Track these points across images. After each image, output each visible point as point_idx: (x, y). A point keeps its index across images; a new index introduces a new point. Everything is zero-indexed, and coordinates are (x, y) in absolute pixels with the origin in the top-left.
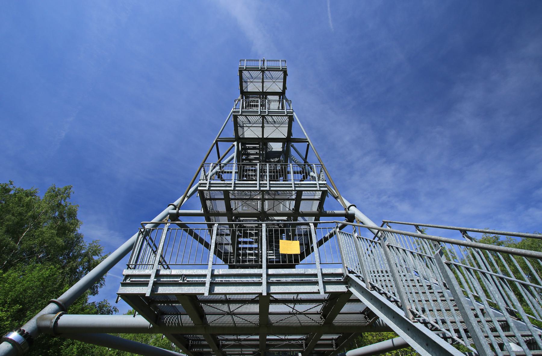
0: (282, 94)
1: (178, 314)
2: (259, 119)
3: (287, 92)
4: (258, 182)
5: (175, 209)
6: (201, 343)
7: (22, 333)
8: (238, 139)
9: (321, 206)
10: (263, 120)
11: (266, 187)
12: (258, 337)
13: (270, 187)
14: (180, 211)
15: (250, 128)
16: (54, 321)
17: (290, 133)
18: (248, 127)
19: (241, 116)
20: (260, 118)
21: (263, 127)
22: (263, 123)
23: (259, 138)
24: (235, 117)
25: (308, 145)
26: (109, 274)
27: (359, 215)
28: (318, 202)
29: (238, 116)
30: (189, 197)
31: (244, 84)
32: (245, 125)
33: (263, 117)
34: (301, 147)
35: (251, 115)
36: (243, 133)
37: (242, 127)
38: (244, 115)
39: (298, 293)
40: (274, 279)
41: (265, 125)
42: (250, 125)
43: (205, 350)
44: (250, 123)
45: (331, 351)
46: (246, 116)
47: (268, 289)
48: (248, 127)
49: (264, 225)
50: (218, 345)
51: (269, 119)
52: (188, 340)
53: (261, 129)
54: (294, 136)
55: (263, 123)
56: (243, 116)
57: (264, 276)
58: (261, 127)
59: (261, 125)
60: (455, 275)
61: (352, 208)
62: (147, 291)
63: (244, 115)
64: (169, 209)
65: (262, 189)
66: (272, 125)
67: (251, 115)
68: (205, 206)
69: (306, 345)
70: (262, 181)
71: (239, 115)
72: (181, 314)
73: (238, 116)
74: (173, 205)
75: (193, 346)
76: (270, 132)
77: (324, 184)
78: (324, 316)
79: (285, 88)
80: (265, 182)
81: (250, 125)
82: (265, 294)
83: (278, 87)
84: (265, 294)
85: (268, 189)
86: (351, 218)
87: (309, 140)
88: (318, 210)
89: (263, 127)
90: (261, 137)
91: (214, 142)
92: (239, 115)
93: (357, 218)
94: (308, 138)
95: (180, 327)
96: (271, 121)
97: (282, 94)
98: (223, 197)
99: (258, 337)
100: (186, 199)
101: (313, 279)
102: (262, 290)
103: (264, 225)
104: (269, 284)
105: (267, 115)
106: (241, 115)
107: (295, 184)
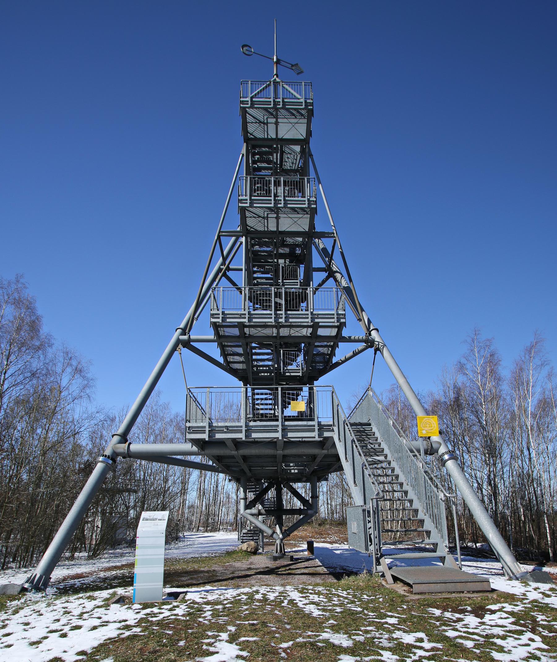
0: (304, 143)
3: (312, 140)
6: (278, 333)
7: (278, 333)
8: (247, 231)
12: (287, 107)
17: (312, 225)
26: (134, 429)
39: (302, 438)
49: (280, 389)
54: (318, 229)
57: (280, 427)
58: (276, 218)
60: (443, 435)
79: (309, 133)
97: (304, 143)
98: (212, 337)
99: (287, 107)
101: (271, 316)
103: (280, 389)
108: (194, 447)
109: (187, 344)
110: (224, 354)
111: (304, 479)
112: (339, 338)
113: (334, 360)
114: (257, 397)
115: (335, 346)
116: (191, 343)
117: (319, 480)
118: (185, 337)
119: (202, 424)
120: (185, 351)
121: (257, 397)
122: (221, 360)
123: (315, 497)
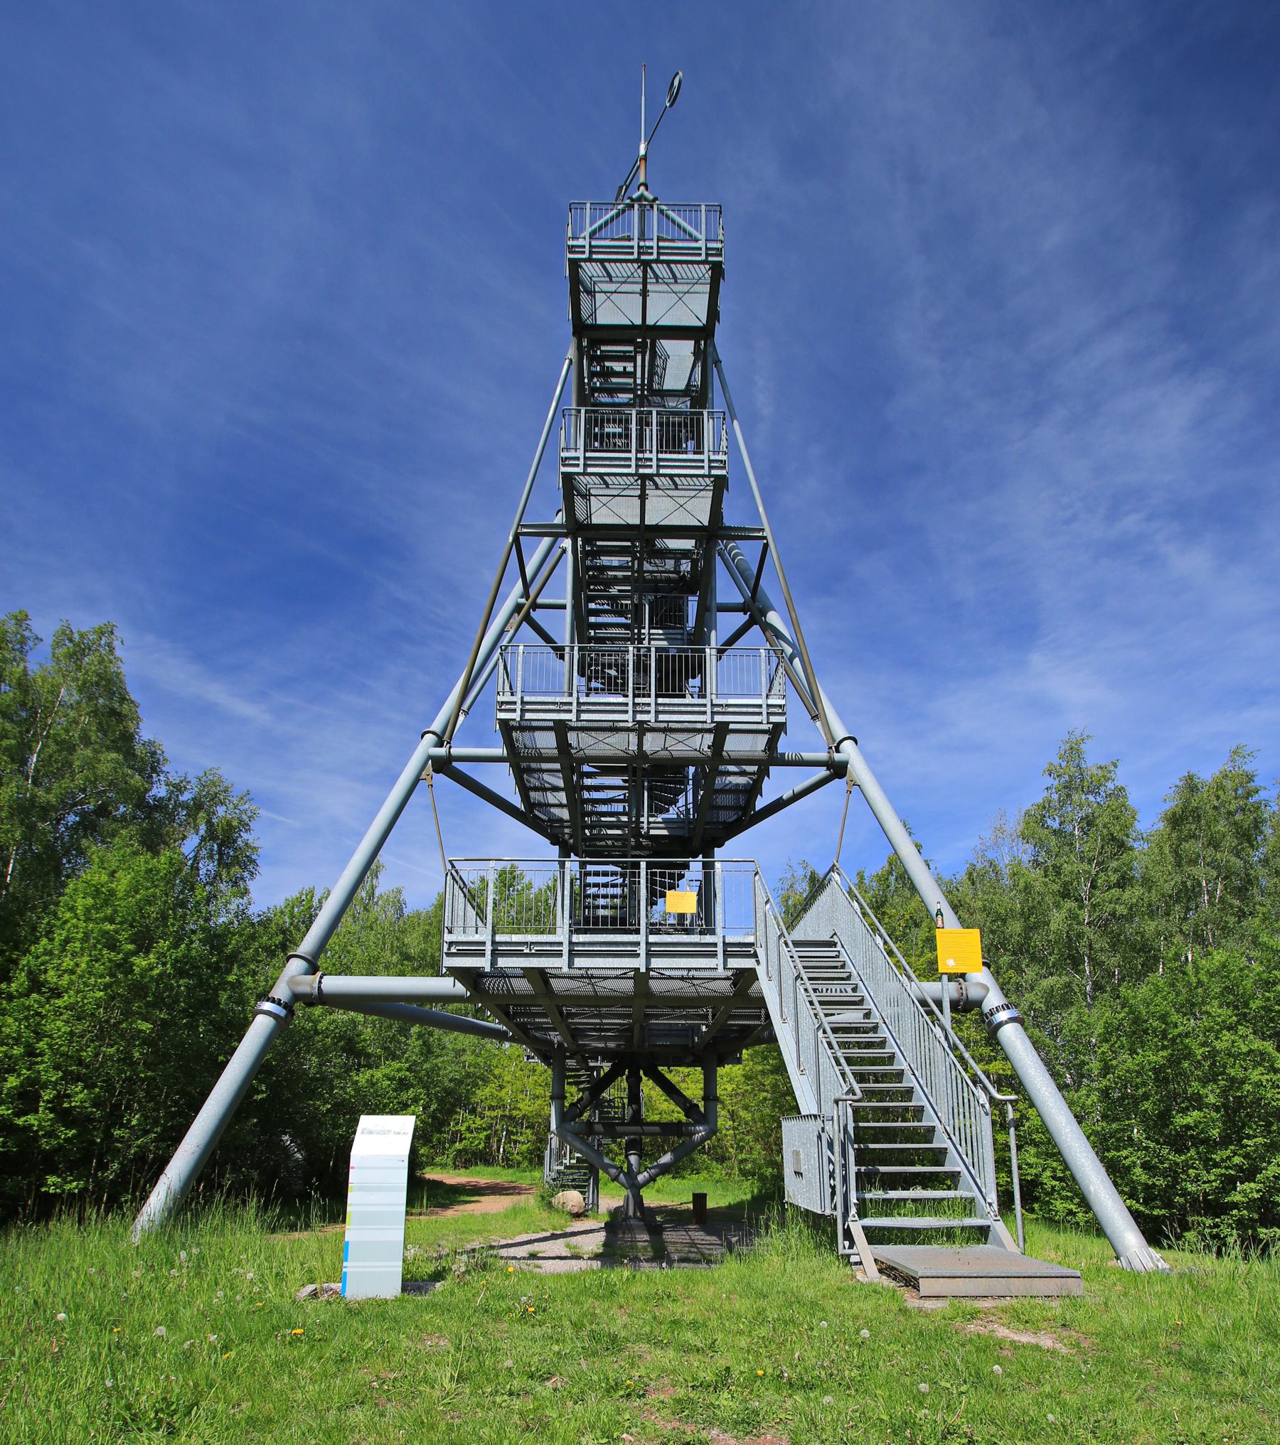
1: (504, 977)
2: (634, 270)
3: (718, 328)
4: (632, 455)
5: (440, 744)
8: (577, 528)
9: (772, 745)
10: (645, 273)
11: (652, 254)
12: (629, 588)
13: (658, 467)
14: (456, 751)
15: (614, 297)
16: (316, 985)
18: (605, 292)
19: (588, 264)
20: (639, 267)
21: (644, 293)
22: (645, 283)
23: (633, 327)
24: (575, 265)
25: (766, 546)
27: (858, 767)
28: (766, 737)
29: (583, 264)
30: (466, 713)
31: (584, 299)
32: (593, 492)
33: (646, 265)
34: (747, 552)
35: (615, 261)
36: (594, 314)
37: (586, 496)
38: (596, 261)
40: (661, 708)
41: (649, 287)
42: (612, 287)
43: (537, 1020)
44: (611, 281)
45: (759, 1025)
46: (602, 262)
47: (648, 962)
48: (605, 292)
50: (561, 1013)
51: (661, 270)
52: (508, 1006)
53: (637, 502)
55: (645, 283)
56: (594, 264)
57: (643, 945)
59: (638, 492)
61: (848, 745)
62: (484, 963)
63: (596, 261)
64: (426, 747)
65: (641, 471)
66: (665, 288)
67: (615, 261)
68: (509, 743)
69: (714, 1016)
70: (642, 452)
71: (585, 260)
72: (509, 977)
73: (583, 264)
74: (434, 733)
75: (516, 1014)
76: (661, 510)
77: (780, 706)
78: (735, 984)
80: (647, 455)
81: (612, 287)
82: (643, 970)
83: (693, 312)
84: (643, 970)
85: (653, 471)
86: (838, 770)
87: (767, 533)
88: (765, 751)
89: (644, 293)
90: (638, 322)
91: (511, 539)
92: (585, 260)
93: (851, 773)
94: (766, 526)
95: (512, 995)
96: (666, 276)
97: (702, 335)
99: (629, 588)
100: (461, 718)
102: (640, 963)
104: (649, 955)
105: (657, 261)
106: (590, 260)
107: (710, 461)
108: (459, 985)
109: (443, 765)
110: (524, 790)
111: (690, 1059)
112: (773, 757)
113: (760, 803)
114: (590, 880)
115: (763, 773)
116: (454, 764)
117: (721, 1063)
118: (442, 751)
119: (477, 938)
120: (441, 778)
121: (590, 880)
122: (516, 800)
123: (710, 1096)
